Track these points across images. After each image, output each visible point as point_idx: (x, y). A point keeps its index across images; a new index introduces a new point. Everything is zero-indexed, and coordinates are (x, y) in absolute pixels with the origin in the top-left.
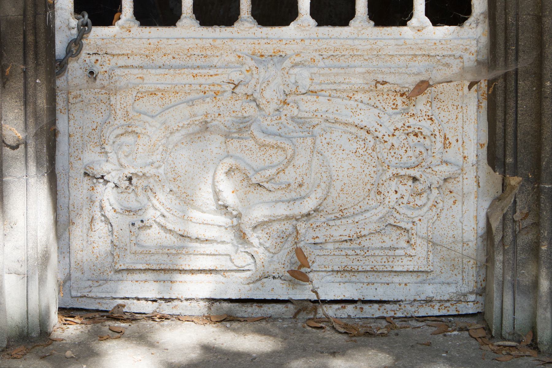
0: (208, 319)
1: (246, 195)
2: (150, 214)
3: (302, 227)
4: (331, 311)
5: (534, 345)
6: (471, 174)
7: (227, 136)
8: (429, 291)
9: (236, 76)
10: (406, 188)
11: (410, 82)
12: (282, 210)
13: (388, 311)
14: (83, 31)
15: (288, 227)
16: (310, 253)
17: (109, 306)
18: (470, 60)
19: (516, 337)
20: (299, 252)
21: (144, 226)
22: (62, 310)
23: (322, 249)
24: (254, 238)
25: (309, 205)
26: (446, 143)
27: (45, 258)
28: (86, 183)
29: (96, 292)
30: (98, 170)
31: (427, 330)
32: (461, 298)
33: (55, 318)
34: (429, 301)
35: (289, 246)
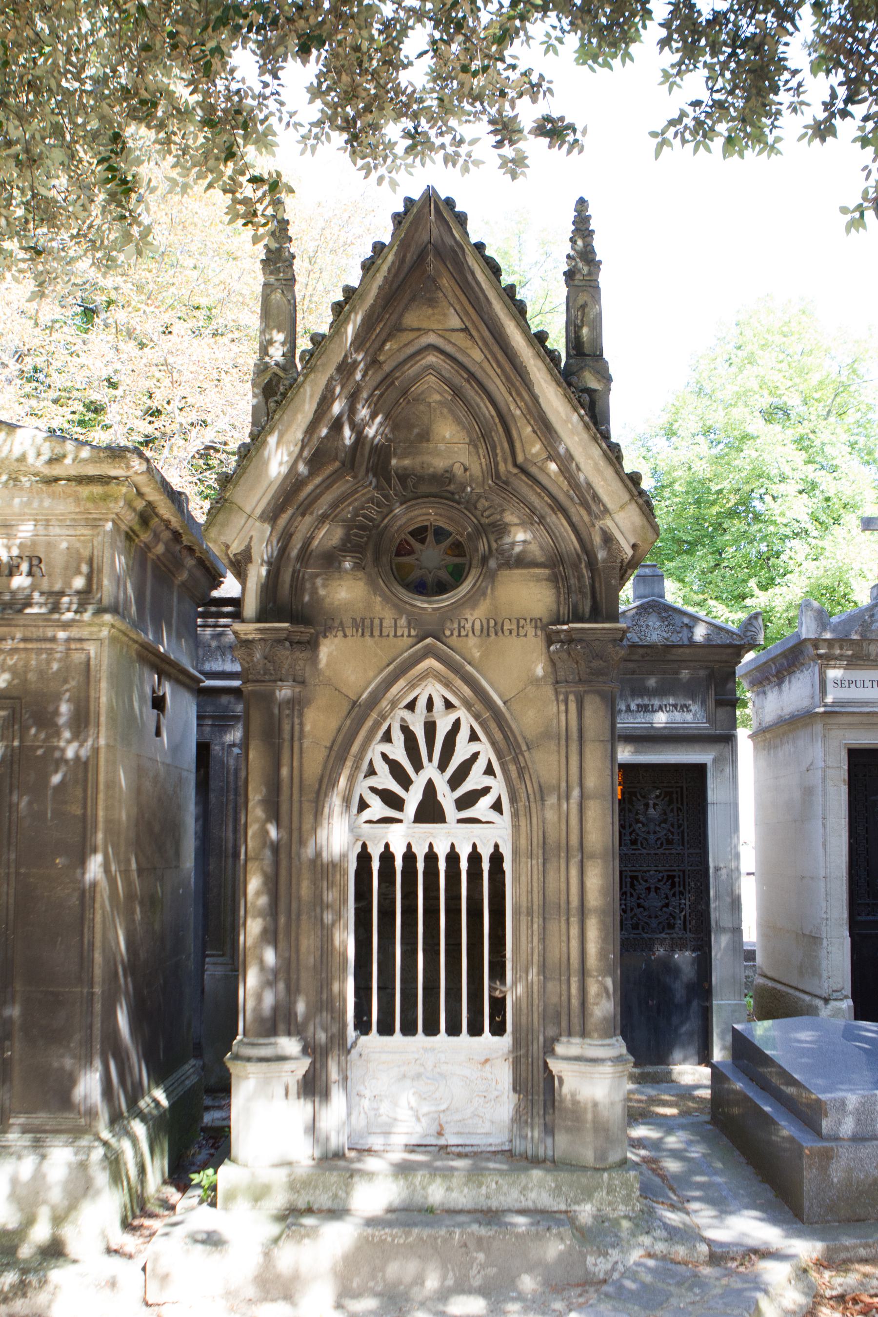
0: (405, 1151)
1: (128, 426)
2: (382, 1111)
3: (442, 1115)
4: (453, 1149)
5: (527, 1158)
6: (506, 1094)
7: (413, 1079)
8: (491, 1140)
9: (416, 1056)
10: (482, 1100)
11: (483, 1060)
12: (433, 1109)
13: (475, 1149)
14: (357, 1038)
15: (436, 1115)
16: (445, 1126)
17: (366, 1147)
18: (506, 1050)
19: (520, 1155)
20: (440, 1125)
21: (380, 1116)
22: (349, 1149)
23: (100, 571)
24: (423, 1120)
25: (443, 1107)
26: (497, 1082)
27: (344, 1124)
28: (357, 1098)
29: (361, 1142)
30: (362, 1093)
31: (489, 1155)
32: (503, 1144)
33: (346, 1151)
34: (491, 1145)
35: (436, 1123)
